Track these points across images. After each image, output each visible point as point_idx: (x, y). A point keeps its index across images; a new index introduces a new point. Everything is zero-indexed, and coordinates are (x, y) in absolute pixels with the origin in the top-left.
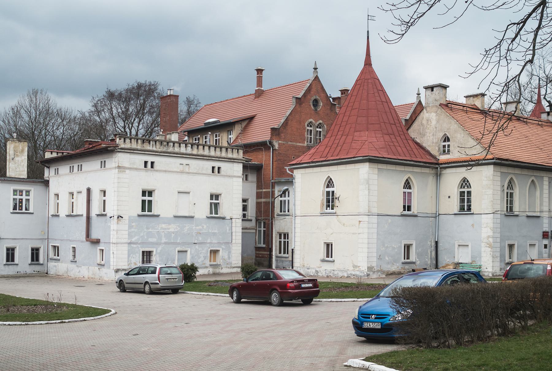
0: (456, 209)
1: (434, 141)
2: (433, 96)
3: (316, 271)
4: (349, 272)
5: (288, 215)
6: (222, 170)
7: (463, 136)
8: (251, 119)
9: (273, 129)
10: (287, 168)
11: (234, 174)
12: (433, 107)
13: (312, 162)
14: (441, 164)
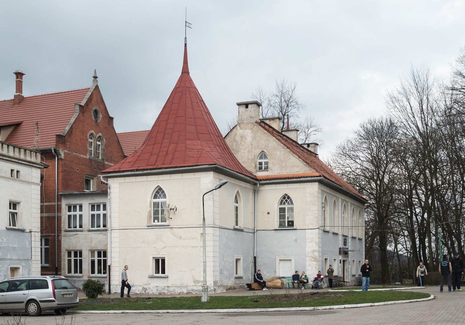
0: (277, 226)
1: (250, 158)
2: (248, 112)
3: (144, 288)
4: (190, 288)
5: (82, 231)
6: (21, 173)
7: (283, 153)
8: (17, 125)
9: (59, 136)
10: (101, 176)
11: (33, 181)
12: (247, 123)
13: (137, 170)
14: (261, 180)
